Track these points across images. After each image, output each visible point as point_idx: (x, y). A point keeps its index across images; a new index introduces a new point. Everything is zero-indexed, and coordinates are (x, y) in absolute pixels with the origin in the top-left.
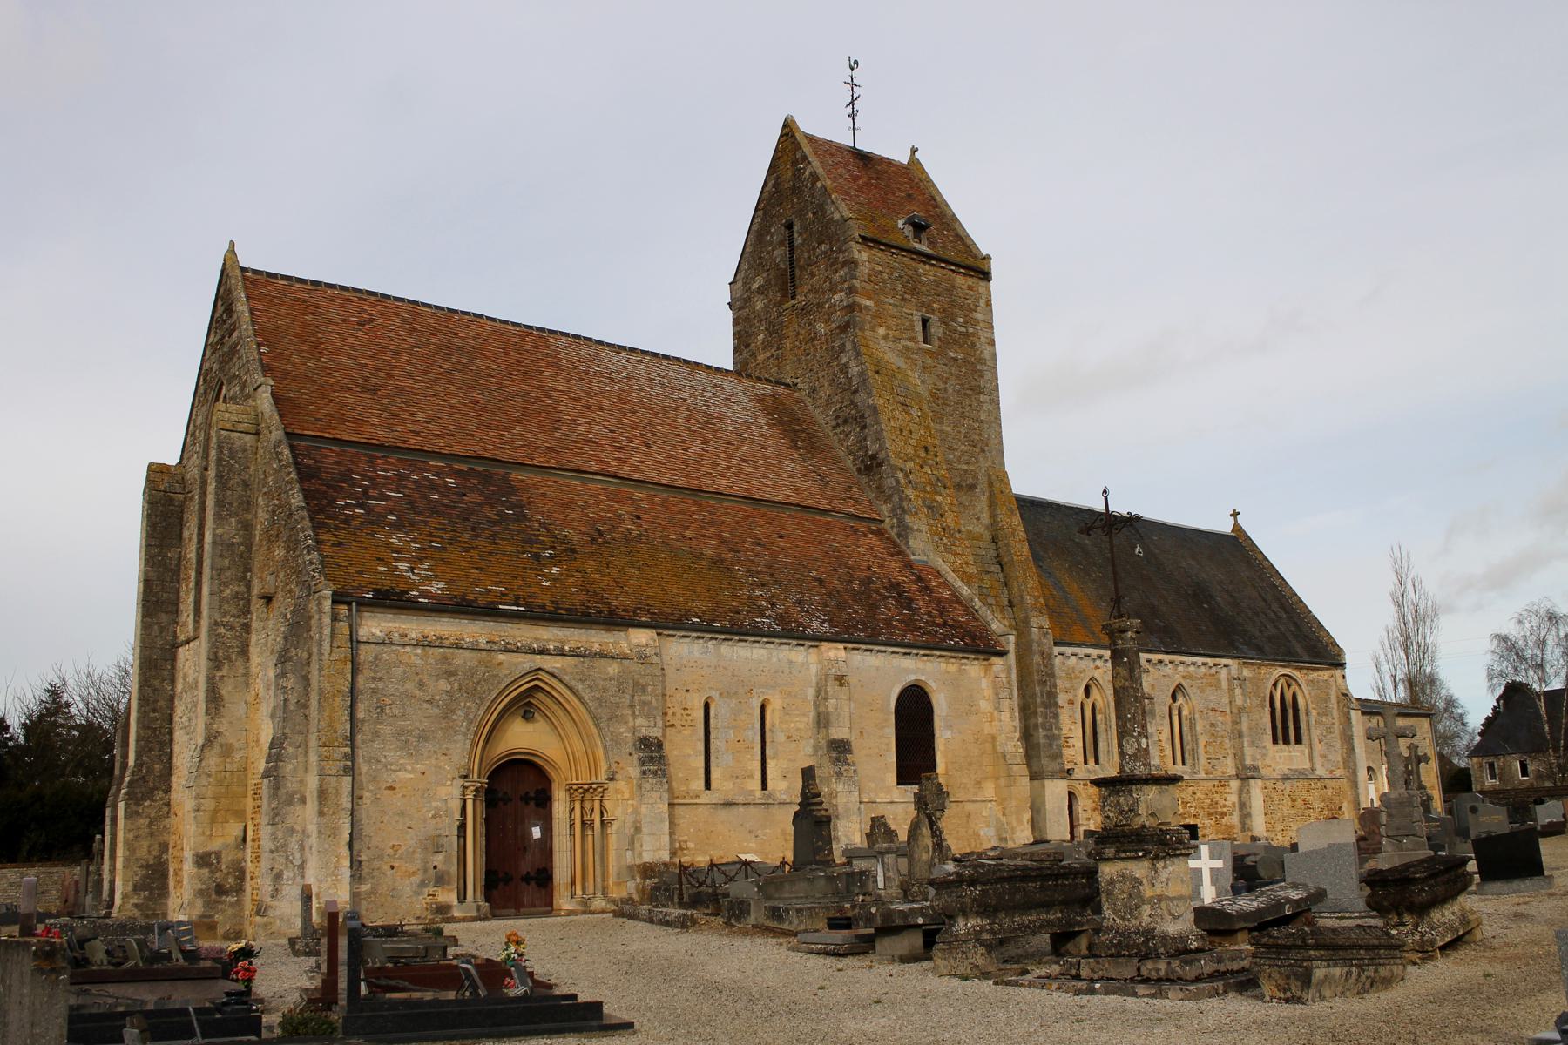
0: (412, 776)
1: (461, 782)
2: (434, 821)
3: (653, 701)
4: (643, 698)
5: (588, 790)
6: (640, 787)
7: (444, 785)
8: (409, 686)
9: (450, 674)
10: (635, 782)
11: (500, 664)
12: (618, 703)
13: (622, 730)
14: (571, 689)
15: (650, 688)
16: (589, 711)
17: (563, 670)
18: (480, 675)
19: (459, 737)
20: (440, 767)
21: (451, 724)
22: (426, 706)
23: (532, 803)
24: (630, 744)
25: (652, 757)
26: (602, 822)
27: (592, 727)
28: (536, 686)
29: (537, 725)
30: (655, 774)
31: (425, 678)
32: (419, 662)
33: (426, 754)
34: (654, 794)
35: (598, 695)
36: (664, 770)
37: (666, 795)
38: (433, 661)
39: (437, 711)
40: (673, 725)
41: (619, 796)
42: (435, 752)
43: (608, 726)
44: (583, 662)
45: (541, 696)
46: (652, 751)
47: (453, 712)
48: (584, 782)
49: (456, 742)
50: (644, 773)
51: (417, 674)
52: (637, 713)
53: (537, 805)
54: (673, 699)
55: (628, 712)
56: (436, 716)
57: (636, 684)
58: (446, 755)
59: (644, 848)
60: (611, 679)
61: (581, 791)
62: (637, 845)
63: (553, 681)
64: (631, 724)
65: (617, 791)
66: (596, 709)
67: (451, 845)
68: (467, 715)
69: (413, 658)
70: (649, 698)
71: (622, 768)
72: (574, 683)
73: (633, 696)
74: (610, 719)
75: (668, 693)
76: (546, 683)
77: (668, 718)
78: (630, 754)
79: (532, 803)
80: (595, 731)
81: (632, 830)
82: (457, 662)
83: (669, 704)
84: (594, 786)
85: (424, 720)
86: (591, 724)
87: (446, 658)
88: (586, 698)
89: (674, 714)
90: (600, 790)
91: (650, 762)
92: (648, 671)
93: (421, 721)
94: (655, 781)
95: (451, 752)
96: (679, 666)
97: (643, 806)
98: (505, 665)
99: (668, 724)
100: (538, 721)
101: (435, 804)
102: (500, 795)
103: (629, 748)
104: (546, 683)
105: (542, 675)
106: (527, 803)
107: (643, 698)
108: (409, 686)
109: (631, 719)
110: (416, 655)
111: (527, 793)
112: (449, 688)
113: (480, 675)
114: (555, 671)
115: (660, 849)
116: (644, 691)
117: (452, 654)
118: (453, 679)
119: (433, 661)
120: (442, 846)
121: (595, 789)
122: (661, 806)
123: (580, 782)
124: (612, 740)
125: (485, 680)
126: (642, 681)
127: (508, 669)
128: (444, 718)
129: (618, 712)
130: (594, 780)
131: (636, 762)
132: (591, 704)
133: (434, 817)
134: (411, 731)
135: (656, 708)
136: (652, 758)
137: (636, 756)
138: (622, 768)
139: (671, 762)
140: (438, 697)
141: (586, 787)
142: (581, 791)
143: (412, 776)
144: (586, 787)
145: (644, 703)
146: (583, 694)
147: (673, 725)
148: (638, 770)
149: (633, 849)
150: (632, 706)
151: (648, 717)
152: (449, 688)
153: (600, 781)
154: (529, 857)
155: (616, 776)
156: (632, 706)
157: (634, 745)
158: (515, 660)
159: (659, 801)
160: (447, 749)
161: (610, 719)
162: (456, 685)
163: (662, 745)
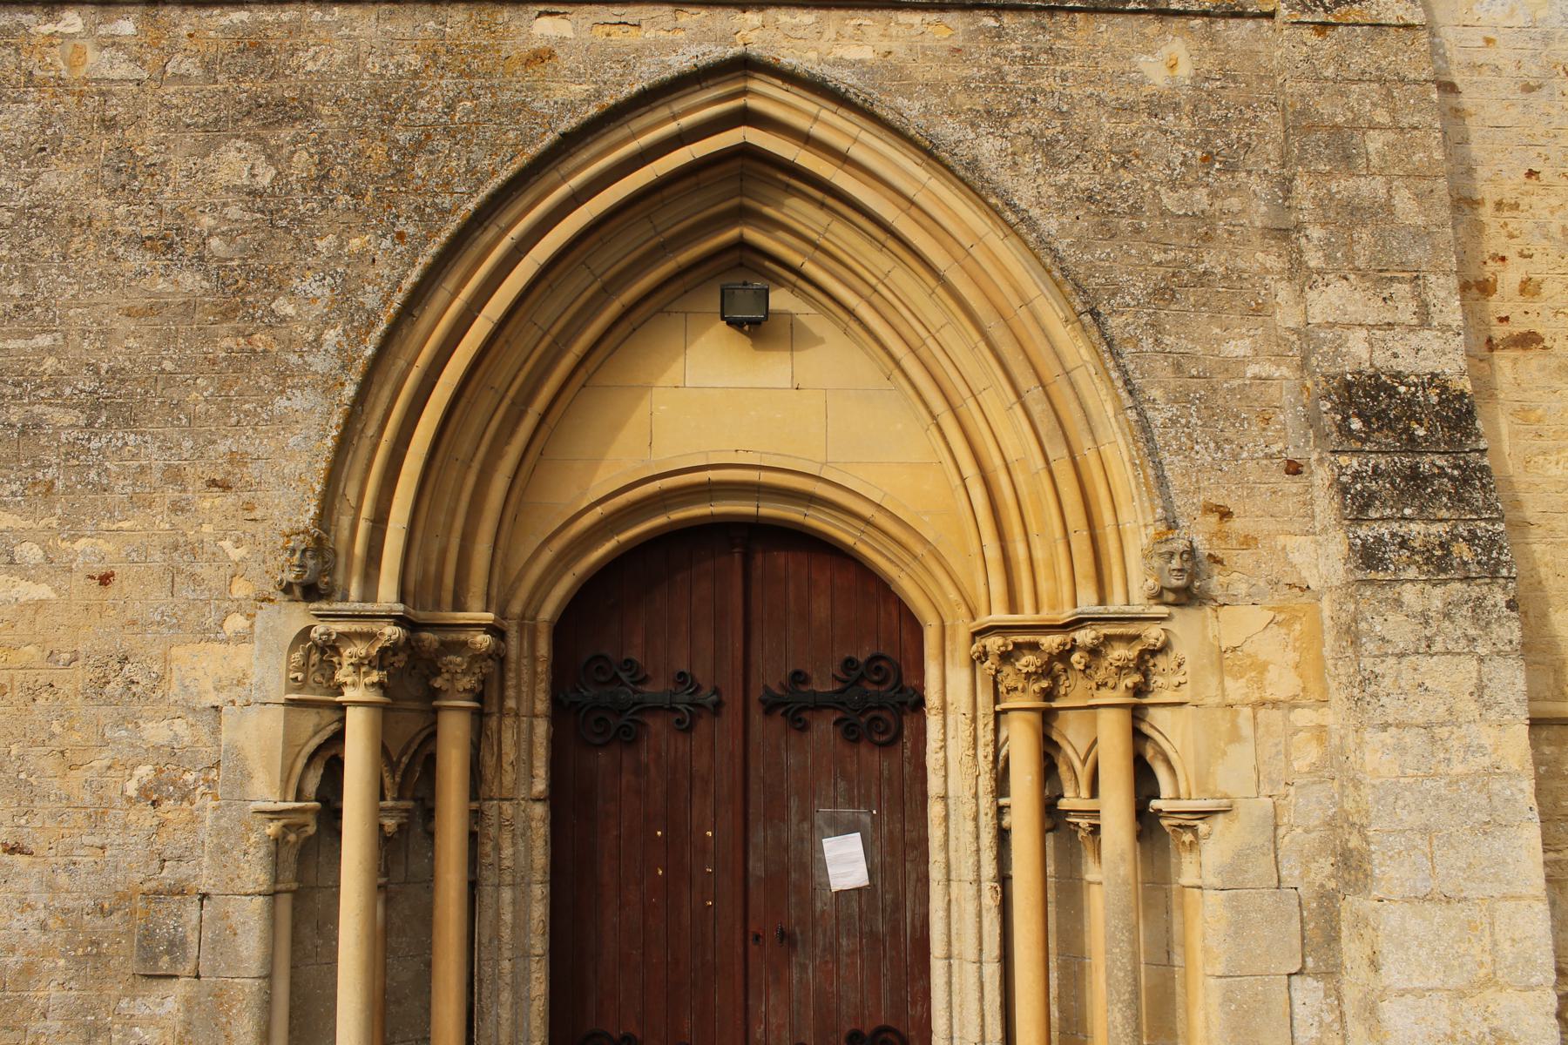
0: (43, 591)
1: (296, 617)
2: (146, 818)
3: (1404, 202)
4: (1342, 186)
5: (1064, 655)
6: (1351, 635)
7: (208, 634)
8: (60, 178)
9: (282, 112)
10: (1326, 607)
11: (541, 57)
12: (1202, 217)
13: (1237, 348)
14: (928, 152)
15: (1375, 143)
16: (1041, 251)
17: (890, 71)
18: (429, 108)
19: (300, 401)
20: (194, 550)
21: (261, 340)
22: (136, 260)
23: (824, 727)
24: (1289, 417)
25: (1414, 475)
26: (1146, 823)
27: (1064, 335)
28: (745, 151)
29: (807, 359)
30: (1438, 561)
31: (146, 142)
32: (123, 70)
33: (122, 488)
34: (1436, 671)
35: (1084, 178)
36: (1493, 542)
37: (1511, 680)
38: (190, 67)
39: (191, 281)
40: (1528, 340)
41: (1236, 689)
42: (174, 476)
43: (1155, 326)
44: (999, 34)
45: (800, 212)
46: (1412, 445)
47: (276, 283)
48: (1046, 616)
49: (283, 422)
50: (1368, 556)
51: (109, 125)
52: (1314, 260)
53: (851, 733)
54: (1518, 222)
55: (1270, 259)
56: (189, 307)
57: (1300, 122)
58: (225, 487)
59: (1392, 975)
60: (1156, 106)
61: (1028, 661)
62: (1352, 950)
63: (834, 125)
64: (1287, 316)
65: (1223, 659)
66: (1081, 243)
67: (225, 939)
68: (345, 294)
69: (92, 56)
70: (1370, 187)
71: (1248, 542)
72: (949, 130)
73: (1286, 185)
74: (1164, 294)
75: (1487, 192)
76: (807, 140)
77: (1496, 305)
78: (1294, 469)
79: (824, 727)
80: (1077, 350)
81: (1323, 870)
82: (311, 62)
83: (1494, 241)
84: (1085, 636)
85: (123, 325)
86: (1052, 312)
87: (260, 50)
88: (1024, 195)
89: (1528, 288)
90: (1119, 653)
91: (1402, 498)
92: (1358, 62)
93: (107, 333)
94: (1437, 597)
95: (252, 471)
96: (1533, 71)
97: (1373, 737)
98: (566, 61)
99: (1500, 332)
100: (818, 341)
101: (156, 732)
102: (656, 688)
103: (1291, 439)
104: (807, 140)
105: (768, 96)
106: (798, 724)
107: (1342, 186)
108: (60, 178)
109: (1284, 292)
110: (115, 43)
111: (799, 677)
112: (265, 177)
113: (429, 108)
114: (844, 79)
115: (1490, 981)
116: (1346, 157)
117: (294, 30)
118: (286, 134)
119: (190, 67)
120: (176, 946)
121: (1095, 652)
122: (1485, 735)
123: (1027, 616)
124: (1181, 398)
125: (449, 132)
126: (1329, 109)
127: (578, 76)
128: (227, 314)
129: (1211, 260)
130: (1088, 603)
131: (1326, 506)
132: (1050, 225)
133: (151, 796)
134: (56, 380)
135: (1421, 235)
136: (1415, 477)
137: (1322, 476)
138: (1248, 542)
139: (1531, 512)
140: (207, 221)
141: (1051, 642)
142: (1028, 661)
143: (43, 591)
144: (1051, 642)
145: (1354, 212)
146: (1005, 179)
147: (1528, 340)
148: (1337, 544)
149: (1331, 973)
150: (1283, 233)
151: (1379, 278)
152: (265, 177)
153: (1116, 605)
154: (805, 973)
155: (1216, 582)
156: (1283, 233)
157: (1312, 420)
158: (634, 37)
159: (1470, 707)
160: (237, 459)
161: (1164, 294)
162: (302, 162)
163: (1470, 414)
